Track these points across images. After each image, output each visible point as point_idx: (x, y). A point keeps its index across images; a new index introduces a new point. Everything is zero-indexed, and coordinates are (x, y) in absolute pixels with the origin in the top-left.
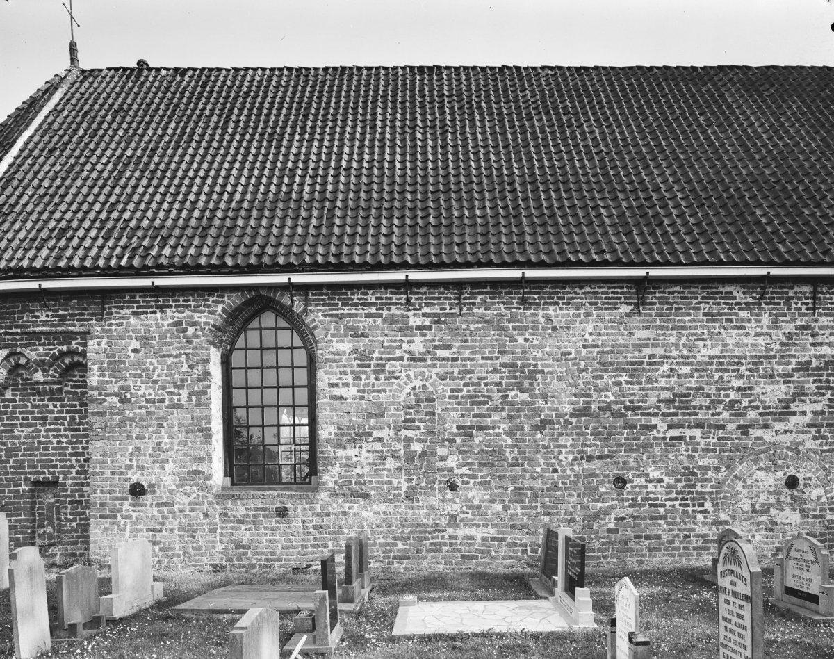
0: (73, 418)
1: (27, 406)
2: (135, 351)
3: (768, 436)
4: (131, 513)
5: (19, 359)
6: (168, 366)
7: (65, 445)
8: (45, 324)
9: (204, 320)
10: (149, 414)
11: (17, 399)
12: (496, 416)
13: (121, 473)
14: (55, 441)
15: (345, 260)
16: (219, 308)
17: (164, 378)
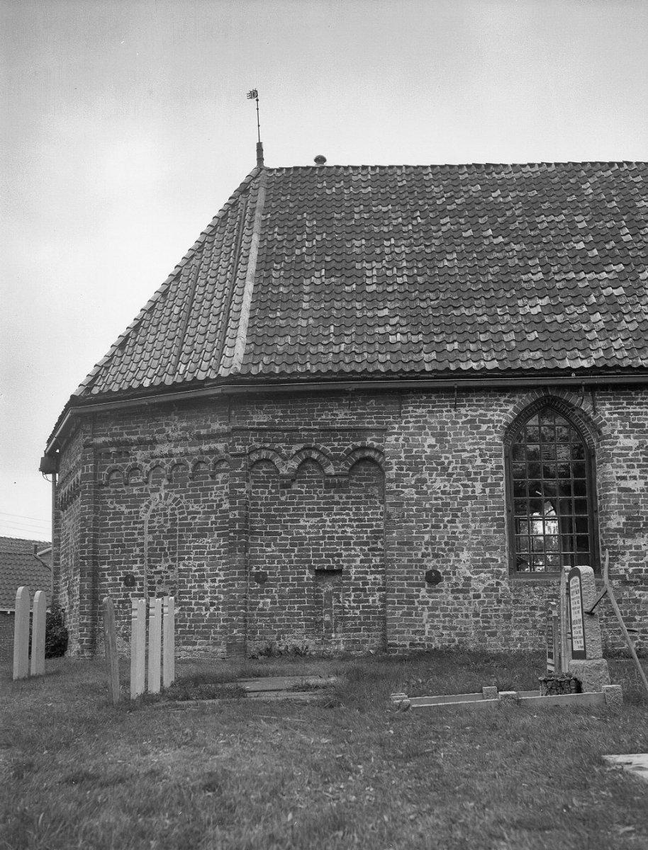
1: (313, 498)
4: (428, 599)
6: (462, 460)
7: (349, 534)
9: (496, 418)
13: (420, 561)
16: (510, 408)
17: (458, 471)
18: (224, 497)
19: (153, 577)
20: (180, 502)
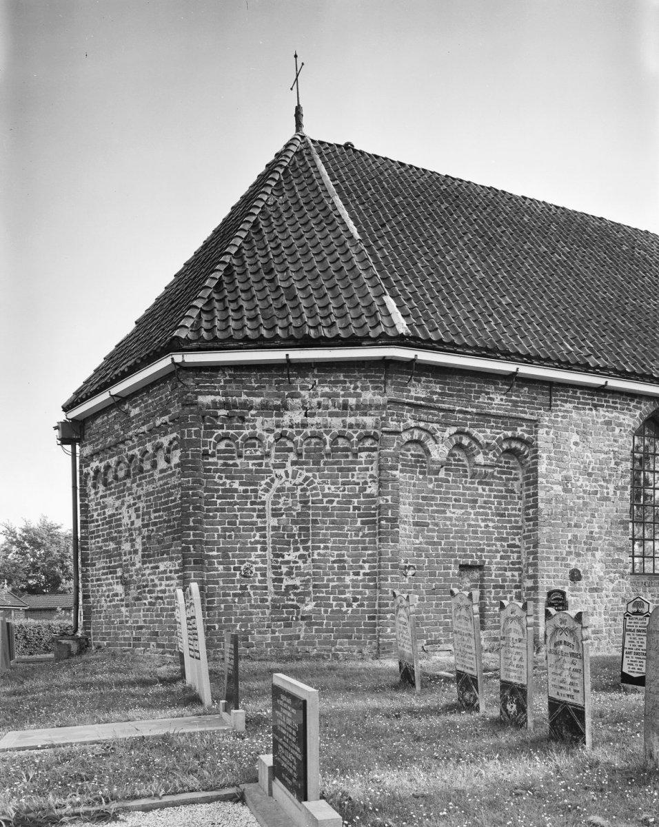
0: (500, 503)
1: (459, 488)
2: (576, 444)
5: (461, 439)
8: (499, 407)
9: (626, 422)
10: (585, 504)
11: (450, 479)
13: (564, 559)
14: (483, 524)
16: (638, 413)
18: (369, 480)
19: (280, 568)
20: (312, 482)
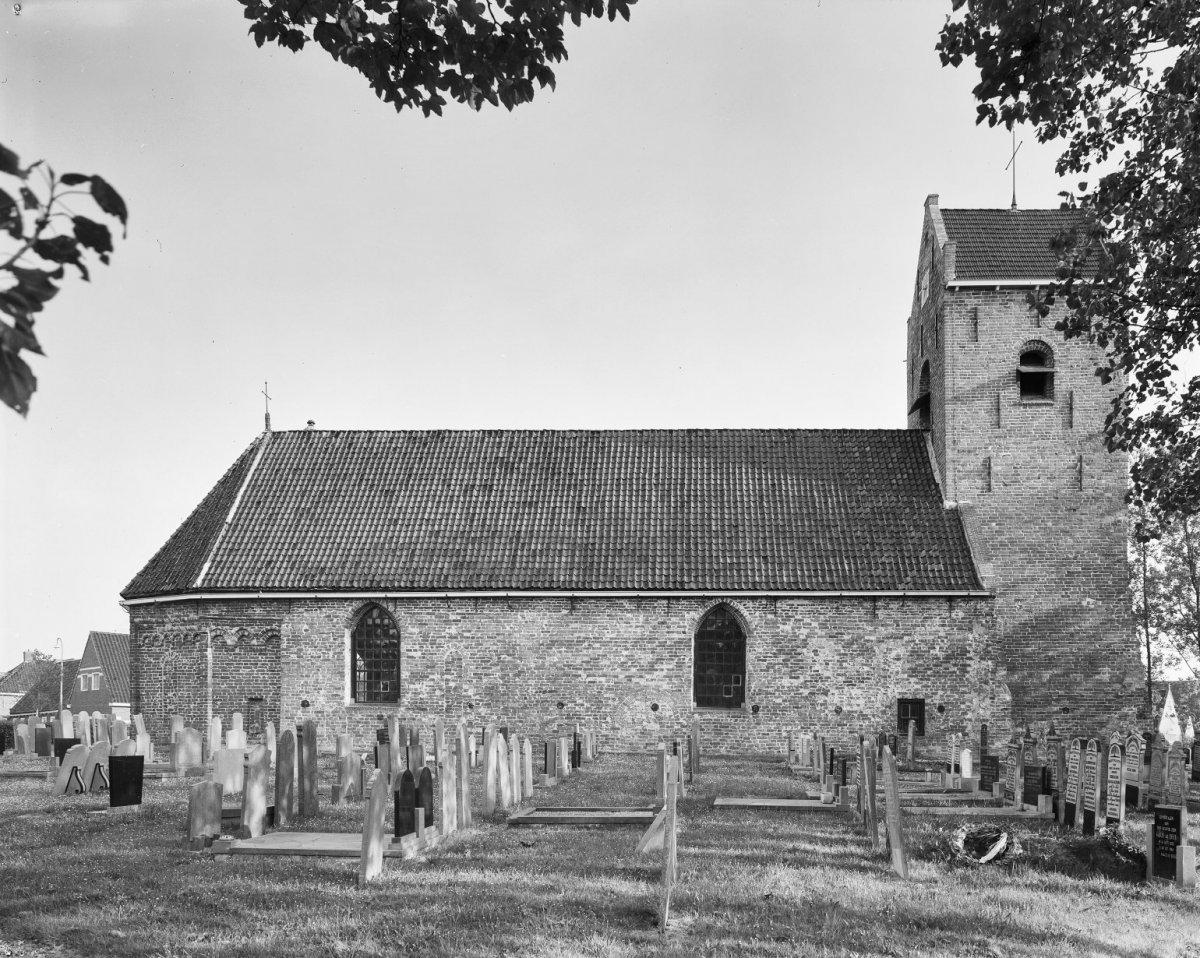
3: (642, 682)
12: (494, 669)
15: (416, 585)
